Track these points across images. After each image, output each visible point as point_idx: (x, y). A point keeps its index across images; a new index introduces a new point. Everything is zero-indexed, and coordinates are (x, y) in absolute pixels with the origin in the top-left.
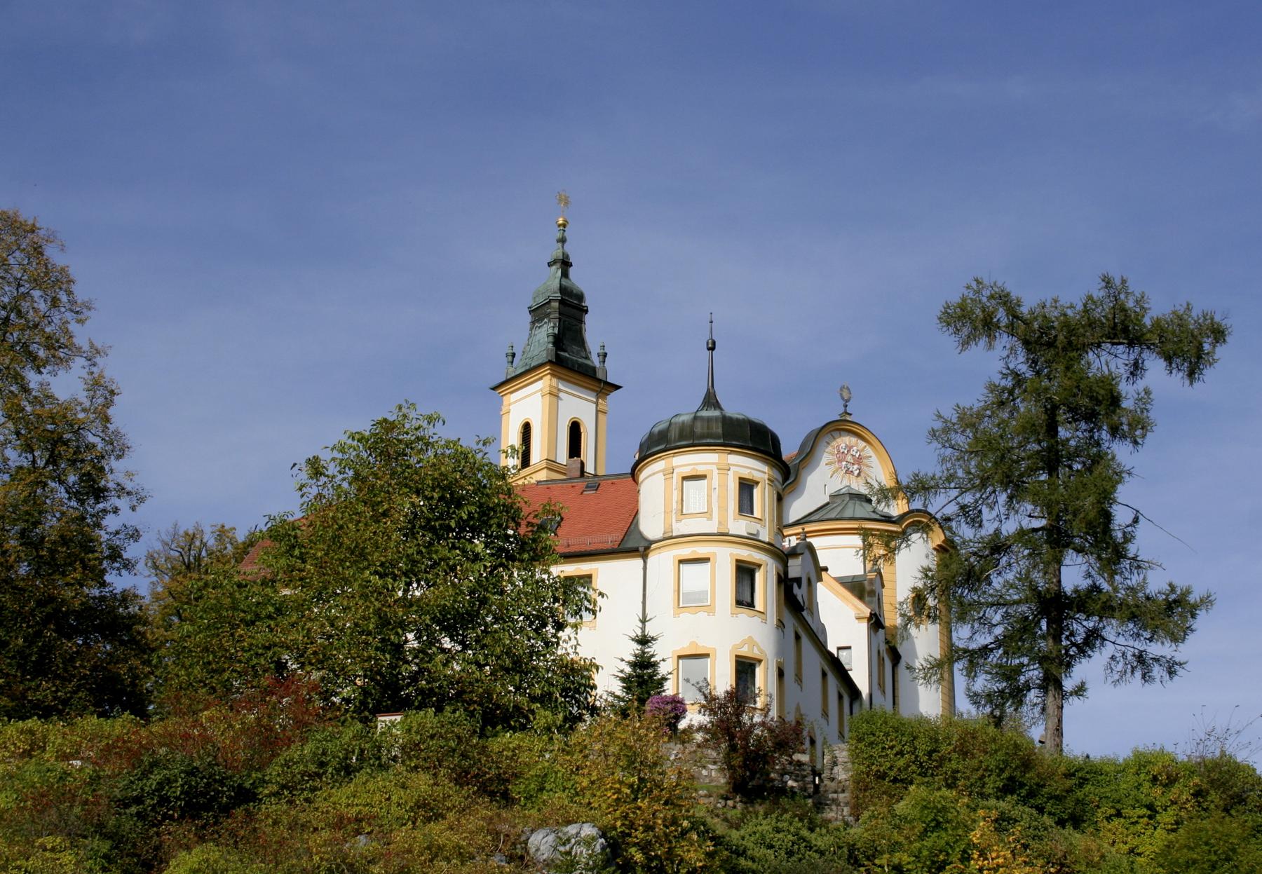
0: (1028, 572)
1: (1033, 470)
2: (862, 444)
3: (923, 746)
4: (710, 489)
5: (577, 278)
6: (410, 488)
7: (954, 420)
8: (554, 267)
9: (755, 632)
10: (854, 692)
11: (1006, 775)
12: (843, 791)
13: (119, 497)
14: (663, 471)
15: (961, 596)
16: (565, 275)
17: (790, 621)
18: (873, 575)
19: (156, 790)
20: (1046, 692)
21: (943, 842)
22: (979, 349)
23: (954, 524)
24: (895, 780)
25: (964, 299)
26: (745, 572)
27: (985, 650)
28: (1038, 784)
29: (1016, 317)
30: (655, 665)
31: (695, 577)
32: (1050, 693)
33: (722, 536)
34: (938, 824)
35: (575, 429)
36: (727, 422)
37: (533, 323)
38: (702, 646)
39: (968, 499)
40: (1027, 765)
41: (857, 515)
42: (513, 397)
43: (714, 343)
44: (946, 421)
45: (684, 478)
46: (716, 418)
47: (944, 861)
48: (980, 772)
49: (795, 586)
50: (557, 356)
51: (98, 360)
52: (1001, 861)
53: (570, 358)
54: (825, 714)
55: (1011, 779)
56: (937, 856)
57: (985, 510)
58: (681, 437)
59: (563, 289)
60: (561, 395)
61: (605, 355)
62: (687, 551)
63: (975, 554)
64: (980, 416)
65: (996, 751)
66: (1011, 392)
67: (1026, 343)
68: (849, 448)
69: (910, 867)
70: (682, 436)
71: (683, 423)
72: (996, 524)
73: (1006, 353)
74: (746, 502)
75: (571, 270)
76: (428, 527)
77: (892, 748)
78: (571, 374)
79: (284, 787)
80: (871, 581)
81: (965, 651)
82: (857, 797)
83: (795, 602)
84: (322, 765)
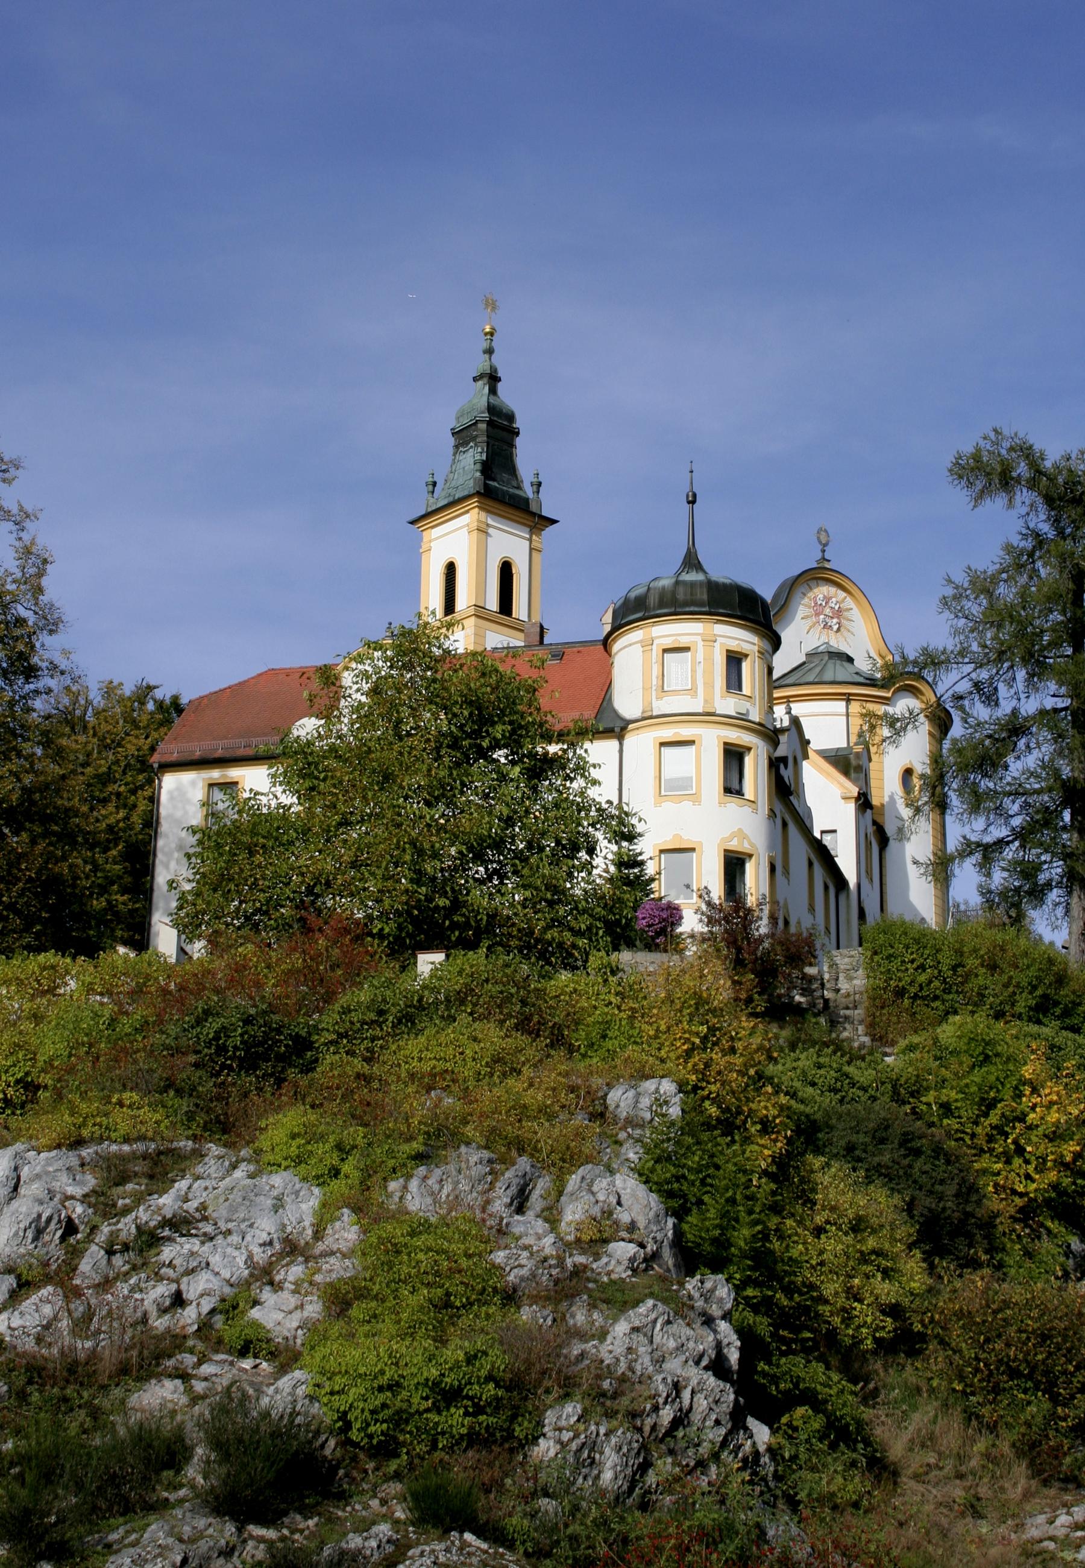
0: (1052, 760)
1: (1055, 644)
2: (842, 594)
3: (946, 960)
4: (694, 663)
5: (508, 396)
6: (436, 704)
7: (966, 585)
8: (480, 383)
9: (745, 823)
10: (841, 882)
11: (1039, 992)
12: (855, 1008)
13: (52, 677)
14: (641, 642)
15: (974, 783)
16: (493, 391)
17: (779, 808)
18: (859, 749)
19: (214, 1039)
20: (1070, 893)
21: (992, 1078)
22: (996, 504)
23: (966, 702)
24: (915, 997)
25: (978, 450)
26: (734, 756)
27: (1001, 843)
28: (1073, 1002)
29: (1039, 472)
30: (642, 863)
31: (677, 761)
32: (1075, 894)
33: (708, 716)
34: (987, 1058)
35: (506, 570)
36: (713, 587)
37: (457, 447)
38: (688, 839)
39: (984, 675)
40: (1061, 980)
41: (840, 678)
42: (436, 532)
43: (694, 495)
44: (957, 587)
45: (665, 651)
46: (701, 583)
47: (994, 1099)
48: (1011, 989)
49: (782, 766)
50: (486, 485)
51: (27, 524)
52: (1055, 1098)
53: (501, 490)
54: (812, 909)
55: (1045, 996)
56: (987, 1093)
57: (1001, 686)
58: (662, 604)
59: (491, 409)
60: (491, 531)
61: (539, 484)
62: (669, 733)
63: (990, 736)
64: (995, 580)
65: (1028, 967)
66: (1031, 555)
67: (1049, 500)
68: (827, 599)
69: (959, 1104)
70: (662, 604)
71: (663, 588)
72: (1014, 703)
73: (1024, 510)
74: (734, 677)
75: (500, 385)
76: (455, 745)
77: (912, 961)
78: (497, 505)
79: (341, 1036)
80: (858, 755)
81: (979, 844)
82: (874, 1015)
83: (785, 790)
84: (381, 1013)
